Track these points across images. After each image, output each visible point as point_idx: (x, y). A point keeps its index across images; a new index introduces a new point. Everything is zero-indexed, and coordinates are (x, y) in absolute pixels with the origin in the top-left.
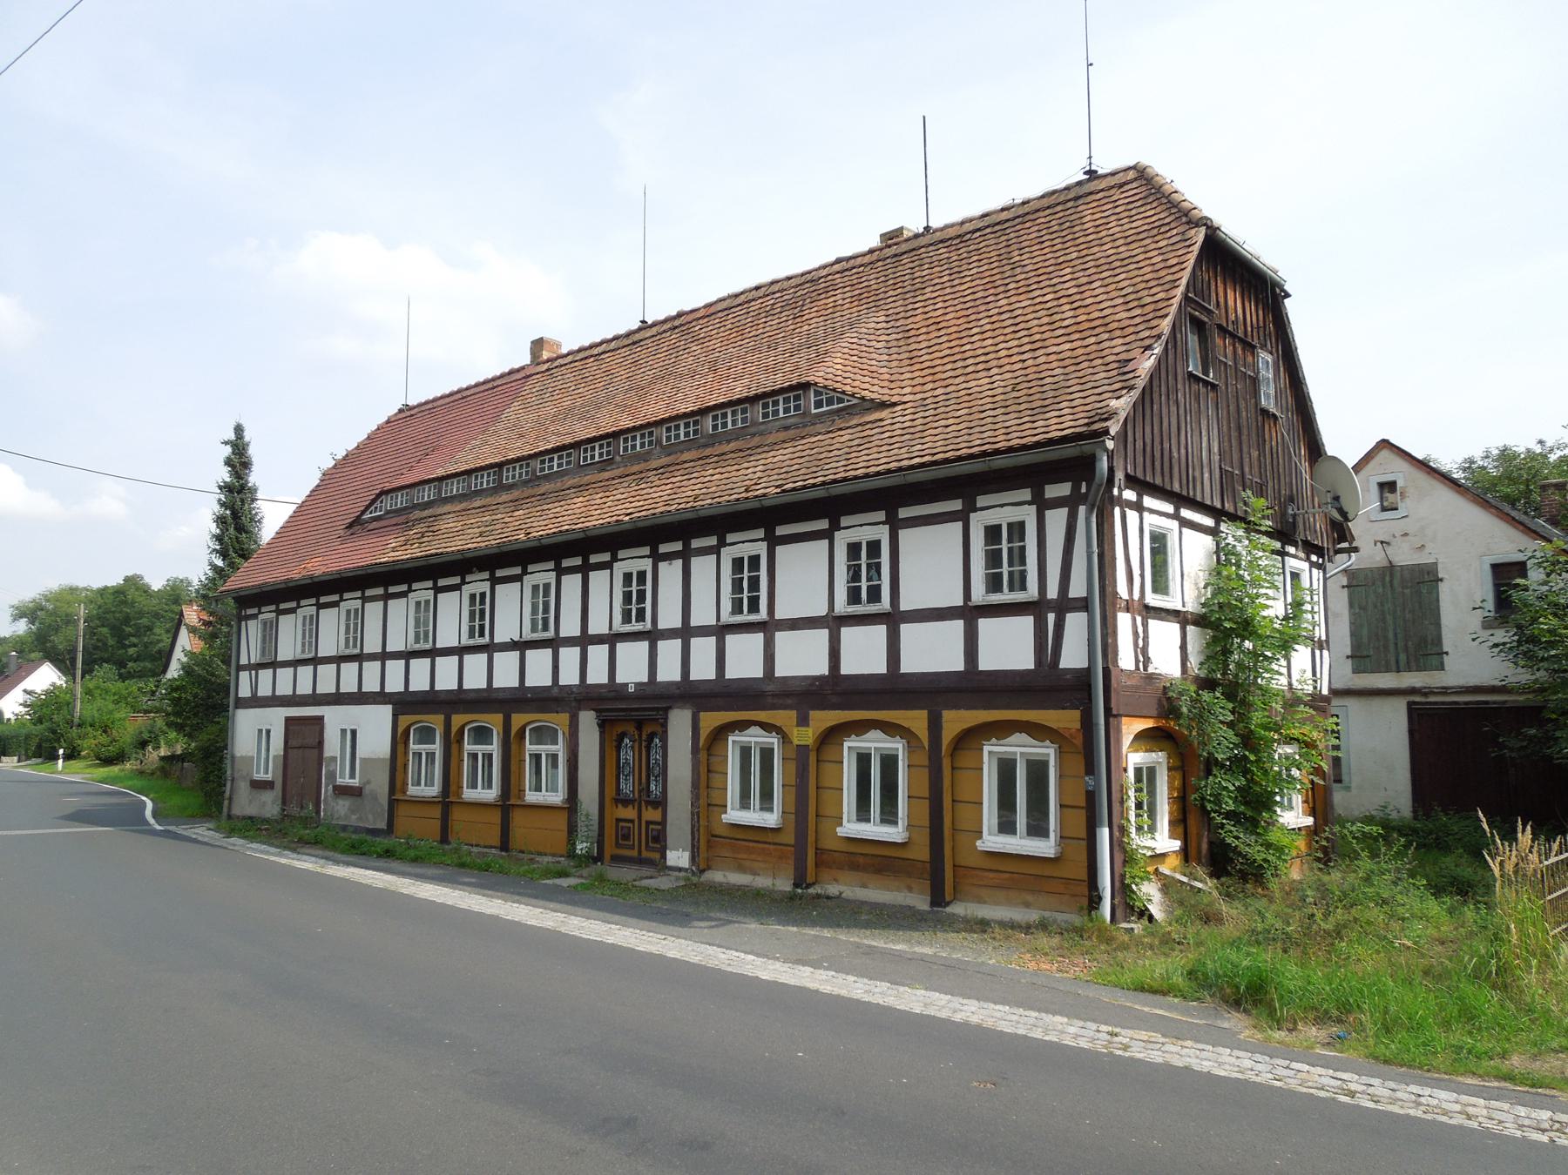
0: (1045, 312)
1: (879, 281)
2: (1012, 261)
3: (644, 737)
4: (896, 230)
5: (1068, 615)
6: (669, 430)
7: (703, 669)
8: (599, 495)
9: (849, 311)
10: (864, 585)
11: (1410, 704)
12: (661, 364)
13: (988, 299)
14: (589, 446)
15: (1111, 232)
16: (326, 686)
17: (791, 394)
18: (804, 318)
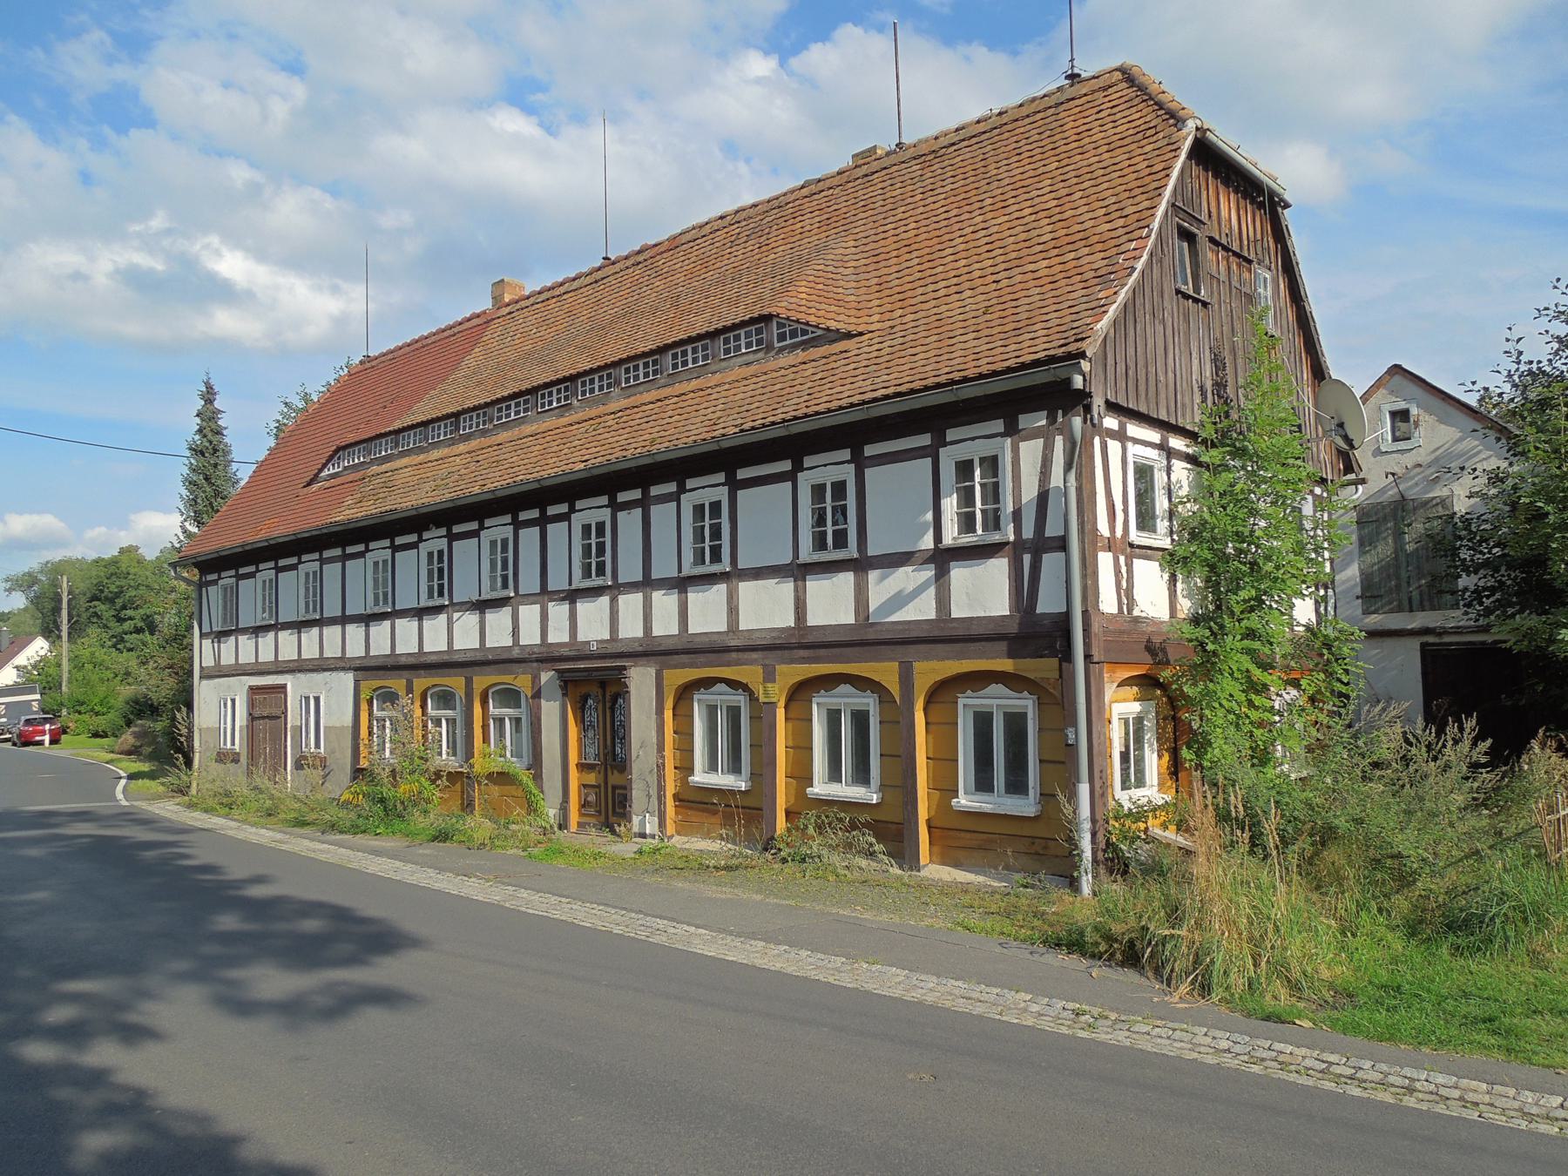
0: (1022, 228)
1: (849, 203)
2: (988, 175)
3: (608, 697)
4: (869, 150)
5: (1044, 555)
6: (627, 371)
7: (665, 625)
8: (556, 443)
9: (817, 237)
10: (830, 529)
11: (1423, 645)
12: (625, 302)
13: (962, 218)
14: (546, 391)
15: (1094, 139)
16: (288, 652)
17: (753, 328)
18: (770, 247)
